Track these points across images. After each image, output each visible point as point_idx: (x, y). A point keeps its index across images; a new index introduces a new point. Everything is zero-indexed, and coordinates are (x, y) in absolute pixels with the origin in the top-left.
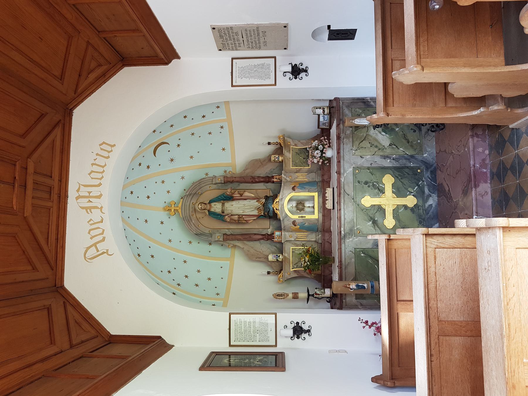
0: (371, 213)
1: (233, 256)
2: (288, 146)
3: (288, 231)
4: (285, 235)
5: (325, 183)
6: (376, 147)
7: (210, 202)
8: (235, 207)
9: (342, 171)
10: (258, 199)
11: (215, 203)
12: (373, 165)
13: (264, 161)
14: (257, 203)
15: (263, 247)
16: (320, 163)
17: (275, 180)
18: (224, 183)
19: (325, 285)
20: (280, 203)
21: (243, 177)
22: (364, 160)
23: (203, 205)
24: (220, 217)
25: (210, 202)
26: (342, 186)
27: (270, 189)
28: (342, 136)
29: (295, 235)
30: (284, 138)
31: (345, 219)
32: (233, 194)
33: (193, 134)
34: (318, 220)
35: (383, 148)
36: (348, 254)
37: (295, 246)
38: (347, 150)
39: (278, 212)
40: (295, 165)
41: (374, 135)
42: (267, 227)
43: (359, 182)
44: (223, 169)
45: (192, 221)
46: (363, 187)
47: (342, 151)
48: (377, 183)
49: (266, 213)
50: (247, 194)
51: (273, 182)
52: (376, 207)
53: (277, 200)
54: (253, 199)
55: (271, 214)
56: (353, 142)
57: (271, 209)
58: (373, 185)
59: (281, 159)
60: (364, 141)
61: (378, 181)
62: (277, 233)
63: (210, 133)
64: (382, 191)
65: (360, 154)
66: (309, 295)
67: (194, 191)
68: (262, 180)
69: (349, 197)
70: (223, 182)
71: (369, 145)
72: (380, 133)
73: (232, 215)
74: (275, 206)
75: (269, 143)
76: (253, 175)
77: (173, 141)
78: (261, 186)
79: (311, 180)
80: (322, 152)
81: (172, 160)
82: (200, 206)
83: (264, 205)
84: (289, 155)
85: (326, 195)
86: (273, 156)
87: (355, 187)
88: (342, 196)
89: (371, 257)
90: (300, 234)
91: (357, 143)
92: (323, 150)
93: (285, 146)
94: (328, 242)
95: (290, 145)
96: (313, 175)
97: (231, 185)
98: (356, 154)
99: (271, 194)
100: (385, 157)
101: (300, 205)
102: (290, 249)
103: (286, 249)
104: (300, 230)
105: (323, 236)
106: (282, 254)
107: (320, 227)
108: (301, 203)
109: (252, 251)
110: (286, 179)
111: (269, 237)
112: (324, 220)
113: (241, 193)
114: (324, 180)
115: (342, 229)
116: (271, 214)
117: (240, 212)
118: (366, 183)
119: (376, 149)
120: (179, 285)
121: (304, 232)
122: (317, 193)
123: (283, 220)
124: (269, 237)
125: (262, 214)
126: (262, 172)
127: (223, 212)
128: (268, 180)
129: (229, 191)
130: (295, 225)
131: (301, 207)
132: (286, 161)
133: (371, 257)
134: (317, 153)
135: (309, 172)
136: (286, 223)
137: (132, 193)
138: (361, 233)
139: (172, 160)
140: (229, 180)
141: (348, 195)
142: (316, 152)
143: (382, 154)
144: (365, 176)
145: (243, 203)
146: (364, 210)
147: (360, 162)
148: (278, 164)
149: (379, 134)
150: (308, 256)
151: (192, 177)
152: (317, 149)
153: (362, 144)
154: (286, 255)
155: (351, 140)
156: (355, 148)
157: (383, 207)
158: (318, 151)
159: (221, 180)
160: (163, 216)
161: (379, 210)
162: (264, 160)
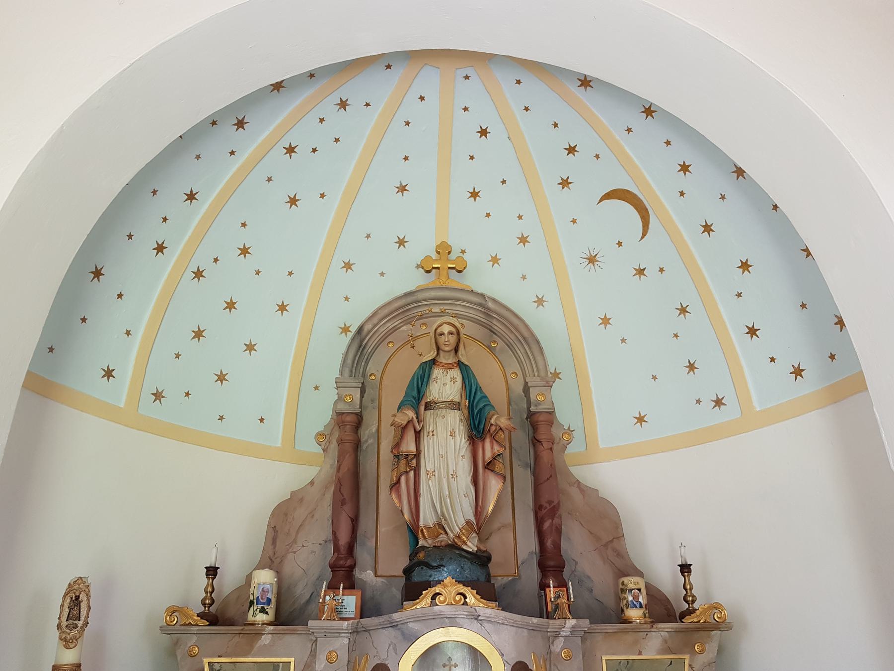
1: (302, 459)
3: (352, 647)
4: (337, 633)
7: (460, 365)
8: (446, 447)
10: (480, 524)
11: (459, 379)
14: (462, 522)
15: (310, 556)
17: (551, 592)
18: (531, 415)
20: (461, 611)
21: (552, 476)
23: (453, 339)
24: (417, 396)
25: (460, 365)
27: (517, 578)
32: (493, 438)
33: (683, 310)
39: (425, 601)
42: (383, 560)
45: (407, 322)
49: (421, 555)
50: (494, 486)
51: (543, 586)
53: (471, 598)
54: (478, 509)
55: (418, 576)
57: (436, 576)
59: (634, 614)
62: (350, 602)
67: (500, 326)
68: (549, 543)
70: (533, 409)
73: (418, 434)
74: (449, 588)
75: (685, 569)
76: (563, 511)
77: (655, 249)
78: (528, 544)
81: (592, 260)
82: (446, 329)
95: (693, 653)
97: (523, 440)
99: (499, 582)
103: (288, 639)
106: (271, 624)
110: (557, 635)
111: (343, 574)
113: (498, 467)
116: (418, 576)
117: (428, 463)
120: (198, 274)
122: (601, 447)
123: (394, 625)
124: (343, 574)
125: (421, 543)
126: (577, 546)
127: (428, 406)
128: (551, 564)
132: (630, 638)
136: (382, 641)
137: (484, 132)
139: (592, 260)
140: (542, 429)
145: (460, 473)
148: (610, 602)
151: (546, 323)
154: (266, 640)
159: (538, 403)
160: (423, 246)
162: (621, 554)
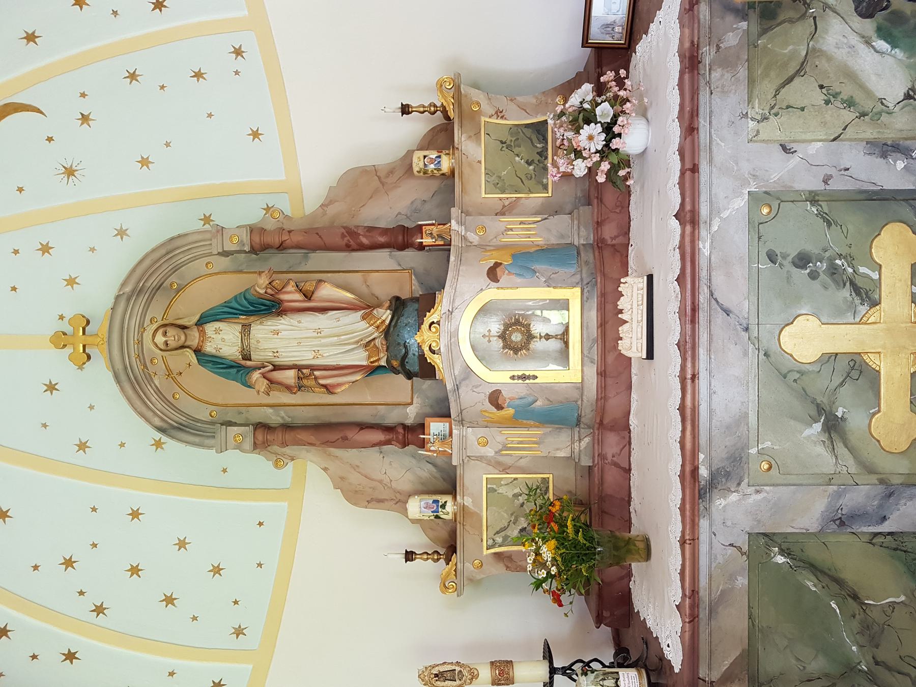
0: (819, 386)
2: (470, 117)
4: (463, 438)
5: (607, 253)
6: (850, 103)
7: (202, 322)
8: (287, 339)
9: (704, 210)
11: (217, 325)
12: (834, 185)
13: (391, 172)
14: (364, 324)
15: (395, 467)
16: (601, 179)
17: (427, 241)
18: (253, 250)
19: (606, 614)
21: (317, 232)
22: (795, 160)
23: (171, 332)
24: (237, 369)
25: (202, 322)
26: (704, 274)
27: (412, 271)
28: (707, 54)
29: (500, 438)
30: (457, 88)
31: (711, 411)
32: (280, 291)
34: (581, 387)
35: (869, 111)
36: (720, 559)
37: (501, 468)
38: (725, 118)
40: (499, 185)
41: (841, 54)
42: (400, 398)
43: (772, 257)
44: (261, 202)
45: (150, 380)
46: (789, 278)
47: (703, 123)
48: (850, 259)
50: (328, 292)
51: (421, 247)
52: (842, 365)
55: (413, 365)
56: (751, 82)
57: (414, 350)
58: (833, 271)
59: (446, 164)
60: (797, 81)
61: (853, 251)
62: (436, 427)
63: (198, 75)
64: (866, 295)
65: (779, 136)
66: (553, 671)
67: (154, 280)
68: (382, 239)
69: (732, 319)
70: (247, 248)
71: (819, 97)
72: (868, 42)
73: (277, 368)
74: (422, 338)
75: (405, 110)
76: (352, 224)
78: (382, 259)
79: (554, 241)
80: (609, 130)
82: (160, 339)
83: (387, 333)
84: (473, 149)
85: (622, 304)
86: (421, 154)
87: (756, 278)
88: (702, 317)
89: (814, 568)
90: (514, 435)
91: (767, 87)
92: (614, 121)
93: (461, 116)
94: (616, 465)
95: (479, 113)
96: (561, 223)
97: (280, 260)
98: (762, 136)
99: (418, 291)
100: (886, 149)
101: (516, 336)
102: (477, 482)
104: (515, 422)
105: (598, 442)
106: (455, 498)
107: (588, 414)
108: (517, 323)
109: (355, 478)
110: (464, 238)
111: (410, 435)
112: (602, 388)
113: (309, 287)
114: (603, 241)
115: (701, 456)
117: (306, 357)
118: (802, 261)
119: (848, 115)
121: (528, 427)
122: (577, 291)
123: (457, 388)
125: (383, 363)
126: (385, 211)
127: (247, 357)
128: (402, 238)
129: (261, 284)
130: (499, 407)
131: (517, 337)
132: (466, 171)
133: (814, 568)
134: (590, 137)
135: (550, 210)
136: (470, 399)
138: (775, 471)
140: (268, 240)
141: (727, 312)
142: (587, 130)
143: (870, 133)
144: (799, 232)
146: (780, 371)
147: (779, 170)
148: (434, 185)
149: (862, 48)
150: (553, 543)
151: (148, 232)
152: (590, 119)
153: (791, 94)
154: (468, 501)
155: (743, 72)
156: (757, 110)
157: (872, 361)
158: (594, 129)
159: (241, 243)
160: (58, 365)
161: (855, 374)
